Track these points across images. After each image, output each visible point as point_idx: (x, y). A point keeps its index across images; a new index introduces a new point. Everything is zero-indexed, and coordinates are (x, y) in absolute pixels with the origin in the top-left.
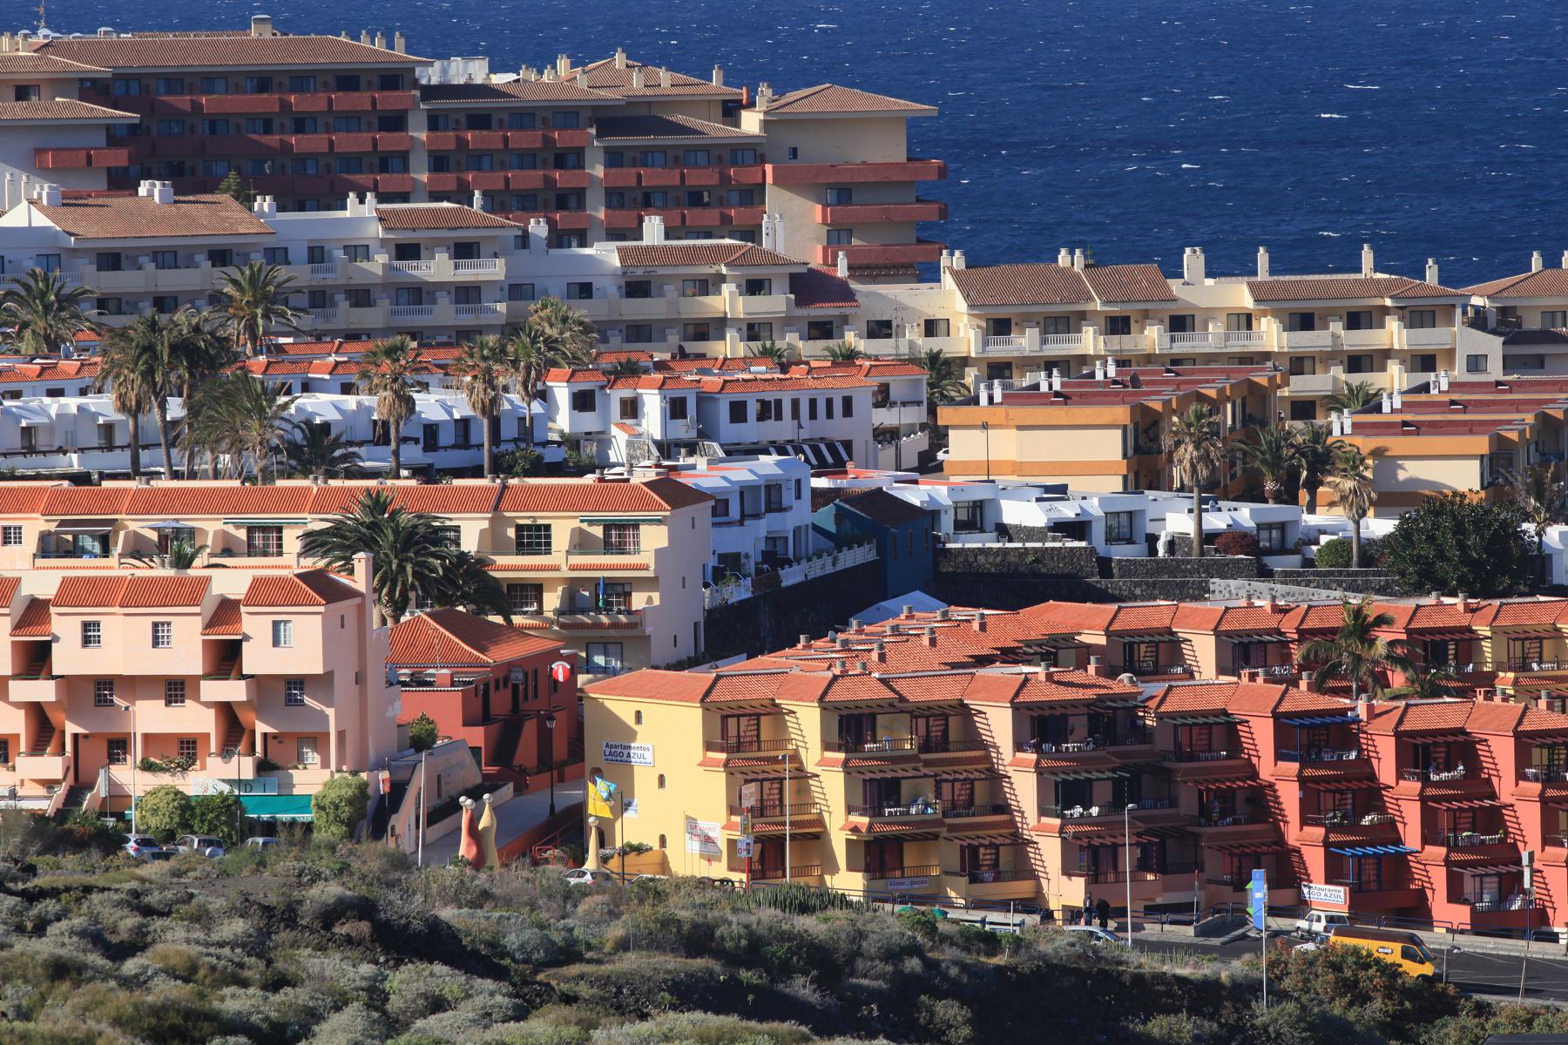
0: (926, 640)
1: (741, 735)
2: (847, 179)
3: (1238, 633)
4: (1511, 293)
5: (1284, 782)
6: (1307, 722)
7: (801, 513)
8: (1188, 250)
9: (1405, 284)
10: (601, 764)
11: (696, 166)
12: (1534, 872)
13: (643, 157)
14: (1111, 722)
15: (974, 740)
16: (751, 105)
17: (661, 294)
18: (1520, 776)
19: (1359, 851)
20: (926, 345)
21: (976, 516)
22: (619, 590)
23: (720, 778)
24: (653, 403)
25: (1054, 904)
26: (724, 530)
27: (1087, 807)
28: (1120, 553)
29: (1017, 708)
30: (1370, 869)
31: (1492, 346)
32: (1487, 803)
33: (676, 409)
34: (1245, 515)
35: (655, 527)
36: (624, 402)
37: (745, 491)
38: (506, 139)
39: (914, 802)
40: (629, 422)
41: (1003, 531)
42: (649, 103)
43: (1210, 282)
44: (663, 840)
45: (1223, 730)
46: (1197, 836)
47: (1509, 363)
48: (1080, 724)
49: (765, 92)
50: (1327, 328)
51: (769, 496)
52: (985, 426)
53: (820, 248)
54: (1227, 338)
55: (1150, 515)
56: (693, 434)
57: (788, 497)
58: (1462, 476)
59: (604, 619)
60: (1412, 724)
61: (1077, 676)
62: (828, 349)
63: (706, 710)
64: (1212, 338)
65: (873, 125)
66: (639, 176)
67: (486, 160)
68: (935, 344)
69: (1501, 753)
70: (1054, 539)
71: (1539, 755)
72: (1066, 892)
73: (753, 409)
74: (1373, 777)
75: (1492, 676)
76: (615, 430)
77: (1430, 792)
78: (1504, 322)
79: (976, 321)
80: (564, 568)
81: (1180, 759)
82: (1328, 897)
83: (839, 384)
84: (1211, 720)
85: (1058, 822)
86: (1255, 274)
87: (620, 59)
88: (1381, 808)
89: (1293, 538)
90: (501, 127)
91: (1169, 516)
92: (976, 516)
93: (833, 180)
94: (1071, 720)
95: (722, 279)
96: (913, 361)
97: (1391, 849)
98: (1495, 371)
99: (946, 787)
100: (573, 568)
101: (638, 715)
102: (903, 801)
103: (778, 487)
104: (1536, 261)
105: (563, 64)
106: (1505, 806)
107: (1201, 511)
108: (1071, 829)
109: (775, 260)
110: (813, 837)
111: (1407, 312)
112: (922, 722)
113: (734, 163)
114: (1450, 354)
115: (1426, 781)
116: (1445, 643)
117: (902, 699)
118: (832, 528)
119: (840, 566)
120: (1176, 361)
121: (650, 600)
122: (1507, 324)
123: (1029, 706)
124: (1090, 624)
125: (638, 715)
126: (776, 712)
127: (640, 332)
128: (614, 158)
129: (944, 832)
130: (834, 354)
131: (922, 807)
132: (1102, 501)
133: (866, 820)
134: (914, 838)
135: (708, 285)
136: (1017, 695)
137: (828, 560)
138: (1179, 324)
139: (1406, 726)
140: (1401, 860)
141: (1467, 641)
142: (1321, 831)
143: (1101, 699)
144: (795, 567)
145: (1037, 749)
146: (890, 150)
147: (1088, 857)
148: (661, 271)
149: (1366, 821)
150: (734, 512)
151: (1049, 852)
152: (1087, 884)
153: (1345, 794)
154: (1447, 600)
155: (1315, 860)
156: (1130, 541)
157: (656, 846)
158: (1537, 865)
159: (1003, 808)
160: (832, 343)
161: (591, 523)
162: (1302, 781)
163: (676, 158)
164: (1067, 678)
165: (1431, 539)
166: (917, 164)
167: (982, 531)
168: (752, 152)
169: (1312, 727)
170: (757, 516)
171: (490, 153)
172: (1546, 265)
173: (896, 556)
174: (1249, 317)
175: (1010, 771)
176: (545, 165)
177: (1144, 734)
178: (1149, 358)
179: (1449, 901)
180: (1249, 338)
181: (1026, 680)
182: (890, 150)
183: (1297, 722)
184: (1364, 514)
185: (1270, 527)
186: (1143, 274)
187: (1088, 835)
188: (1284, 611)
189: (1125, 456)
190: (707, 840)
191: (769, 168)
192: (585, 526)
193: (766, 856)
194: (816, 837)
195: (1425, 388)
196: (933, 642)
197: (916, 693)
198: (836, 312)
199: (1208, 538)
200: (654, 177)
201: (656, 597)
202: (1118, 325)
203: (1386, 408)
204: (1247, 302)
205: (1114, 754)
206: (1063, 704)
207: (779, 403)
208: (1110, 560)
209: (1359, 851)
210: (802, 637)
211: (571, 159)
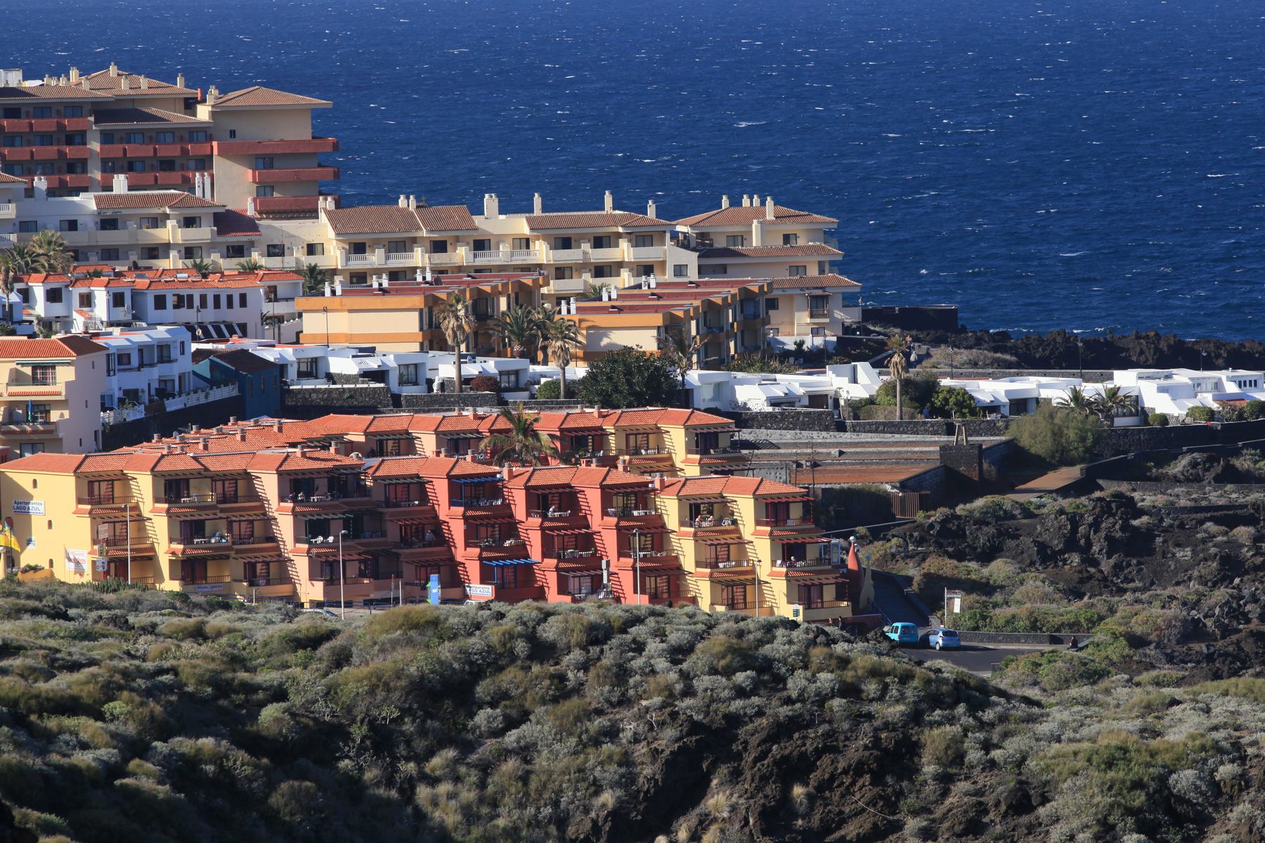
0: (238, 437)
1: (100, 495)
2: (269, 151)
3: (451, 433)
4: (707, 223)
5: (454, 521)
6: (469, 481)
7: (183, 365)
8: (487, 196)
9: (632, 217)
10: (12, 514)
11: (165, 143)
12: (610, 574)
13: (128, 137)
14: (342, 483)
15: (253, 495)
16: (204, 101)
17: (125, 227)
18: (605, 513)
19: (501, 563)
20: (307, 261)
21: (312, 368)
22: (41, 408)
23: (86, 522)
24: (101, 297)
25: (304, 599)
26: (127, 373)
27: (326, 537)
28: (408, 391)
29: (280, 474)
30: (509, 574)
31: (691, 259)
32: (584, 531)
33: (117, 300)
34: (491, 365)
35: (65, 368)
36: (81, 296)
37: (142, 349)
38: (31, 125)
39: (214, 536)
40: (85, 309)
41: (330, 377)
42: (134, 101)
43: (503, 217)
44: (51, 562)
45: (417, 486)
46: (398, 555)
47: (702, 270)
48: (322, 484)
49: (213, 91)
50: (579, 247)
51: (162, 352)
52: (325, 310)
53: (250, 200)
54: (512, 255)
55: (429, 366)
56: (129, 317)
57: (175, 353)
58: (645, 341)
59: (29, 429)
60: (538, 480)
61: (322, 454)
62: (240, 264)
63: (78, 477)
64: (502, 255)
65: (289, 115)
66: (125, 150)
67: (18, 140)
68: (313, 260)
69: (592, 500)
70: (363, 382)
71: (619, 501)
72: (310, 591)
73: (170, 301)
74: (511, 516)
75: (616, 458)
76: (75, 315)
77: (547, 524)
78: (703, 245)
79: (341, 245)
80: (5, 395)
81: (388, 507)
82: (481, 592)
83: (236, 287)
84: (409, 481)
85: (306, 546)
86: (532, 211)
87: (113, 70)
88: (517, 537)
89: (523, 380)
90: (27, 117)
91: (440, 367)
92: (312, 368)
93: (259, 152)
94: (317, 482)
95: (167, 217)
96: (298, 272)
97: (522, 561)
98: (693, 275)
99: (235, 526)
100: (10, 395)
101: (35, 482)
102: (207, 534)
103: (168, 346)
104: (725, 202)
105: (74, 73)
106: (595, 533)
107: (460, 363)
108: (315, 551)
109: (204, 205)
110: (147, 559)
111: (633, 236)
112: (219, 484)
113: (191, 141)
114: (663, 263)
115: (544, 517)
116: (586, 438)
117: (206, 469)
118: (208, 376)
119: (211, 399)
120: (479, 270)
121: (62, 415)
122: (703, 244)
123: (289, 473)
124: (355, 429)
125: (35, 482)
126: (124, 479)
127: (111, 254)
128: (107, 138)
129: (232, 554)
130: (243, 267)
131: (219, 538)
132: (397, 357)
133: (181, 547)
134: (213, 558)
135: (157, 221)
136: (281, 465)
137: (201, 395)
138: (480, 245)
139: (532, 483)
140: (529, 568)
141: (599, 436)
142: (477, 550)
143: (336, 468)
144: (177, 399)
145: (294, 500)
146: (300, 131)
147: (324, 569)
148: (125, 212)
149: (507, 543)
150: (135, 361)
151: (301, 567)
152: (325, 586)
153: (492, 527)
154: (588, 410)
155: (473, 569)
156: (416, 383)
157: (47, 566)
158: (611, 569)
159: (272, 538)
160: (243, 260)
161: (23, 365)
162: (466, 519)
163: (151, 138)
164: (316, 455)
165: (610, 379)
166: (318, 141)
167: (316, 377)
168: (202, 133)
169: (477, 485)
170: (151, 365)
171: (20, 135)
172: (731, 205)
173: (256, 391)
174: (527, 240)
175: (276, 515)
176: (59, 143)
177: (364, 490)
178: (460, 269)
179: (559, 593)
180: (529, 254)
181: (288, 456)
182: (300, 131)
183: (463, 481)
184: (567, 363)
185: (508, 373)
186: (456, 212)
187: (326, 555)
188: (482, 418)
189: (421, 329)
190: (77, 563)
191: (215, 144)
192: (19, 367)
193: (118, 566)
194: (150, 558)
195: (639, 286)
196: (243, 438)
197: (215, 466)
198: (246, 239)
199: (466, 381)
200: (136, 150)
201: (66, 414)
202: (439, 246)
203: (605, 298)
204: (526, 230)
205: (346, 503)
206: (311, 471)
207: (190, 297)
208: (400, 396)
209: (501, 563)
210: (155, 436)
211: (77, 138)
